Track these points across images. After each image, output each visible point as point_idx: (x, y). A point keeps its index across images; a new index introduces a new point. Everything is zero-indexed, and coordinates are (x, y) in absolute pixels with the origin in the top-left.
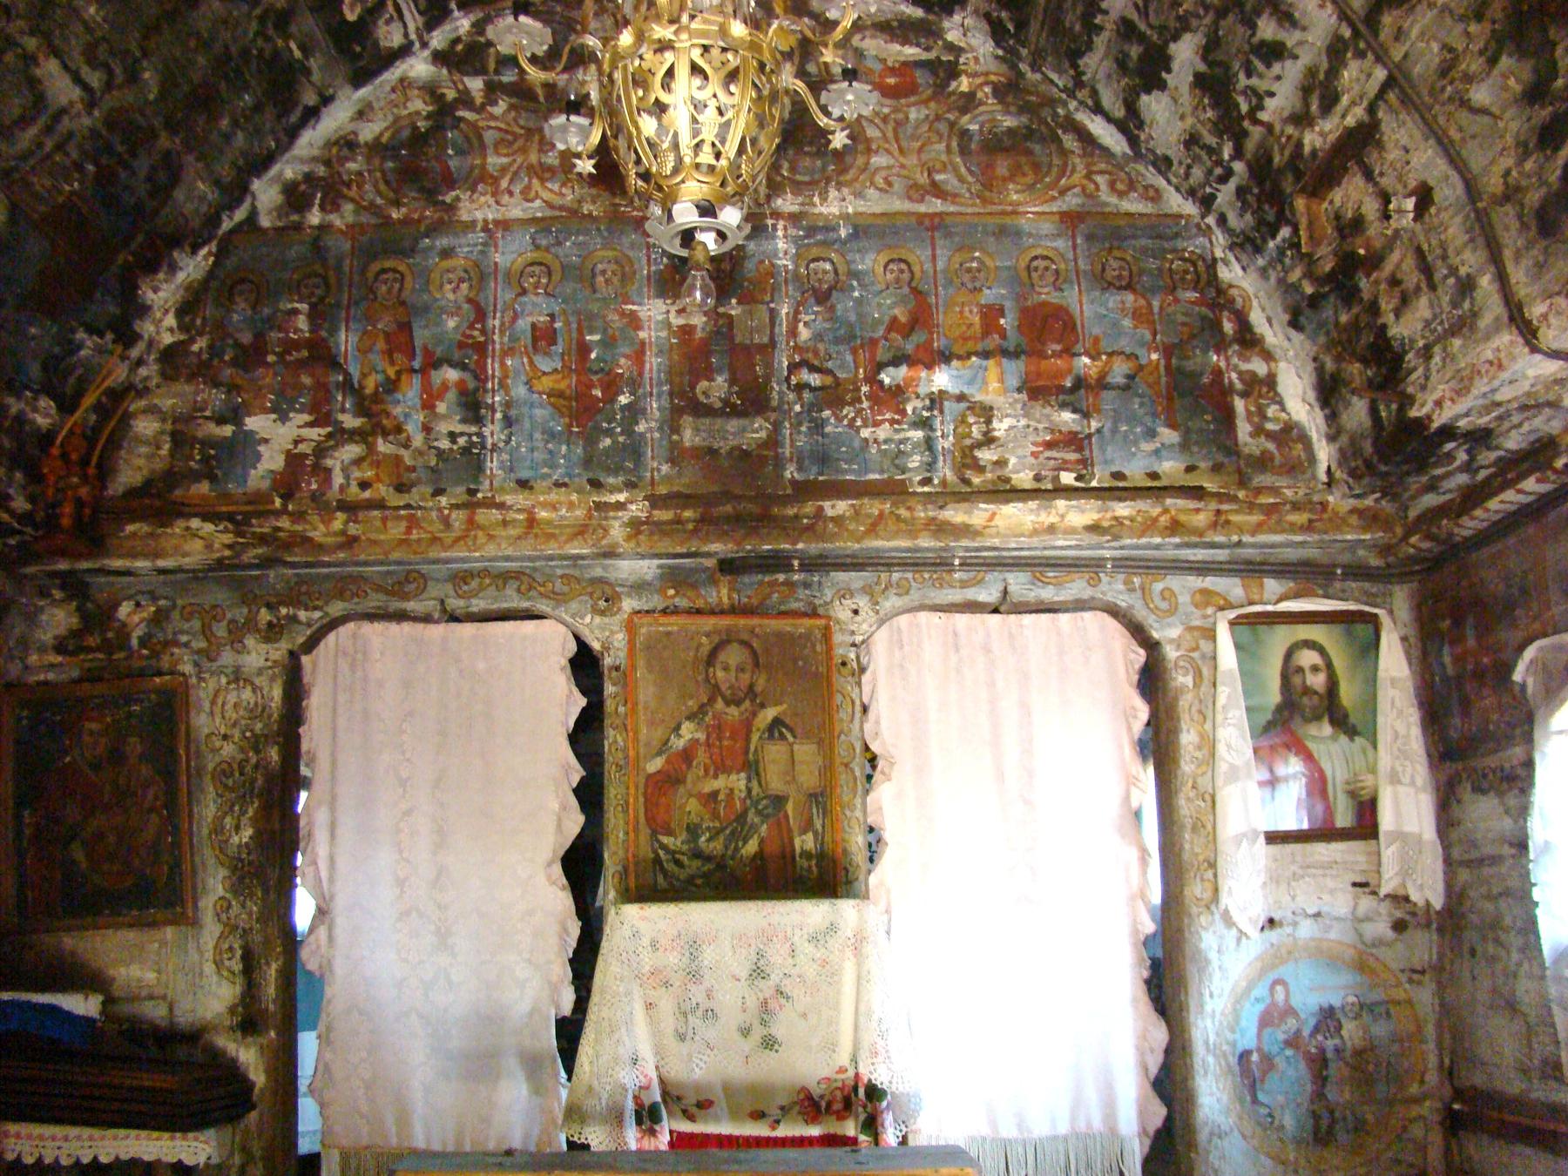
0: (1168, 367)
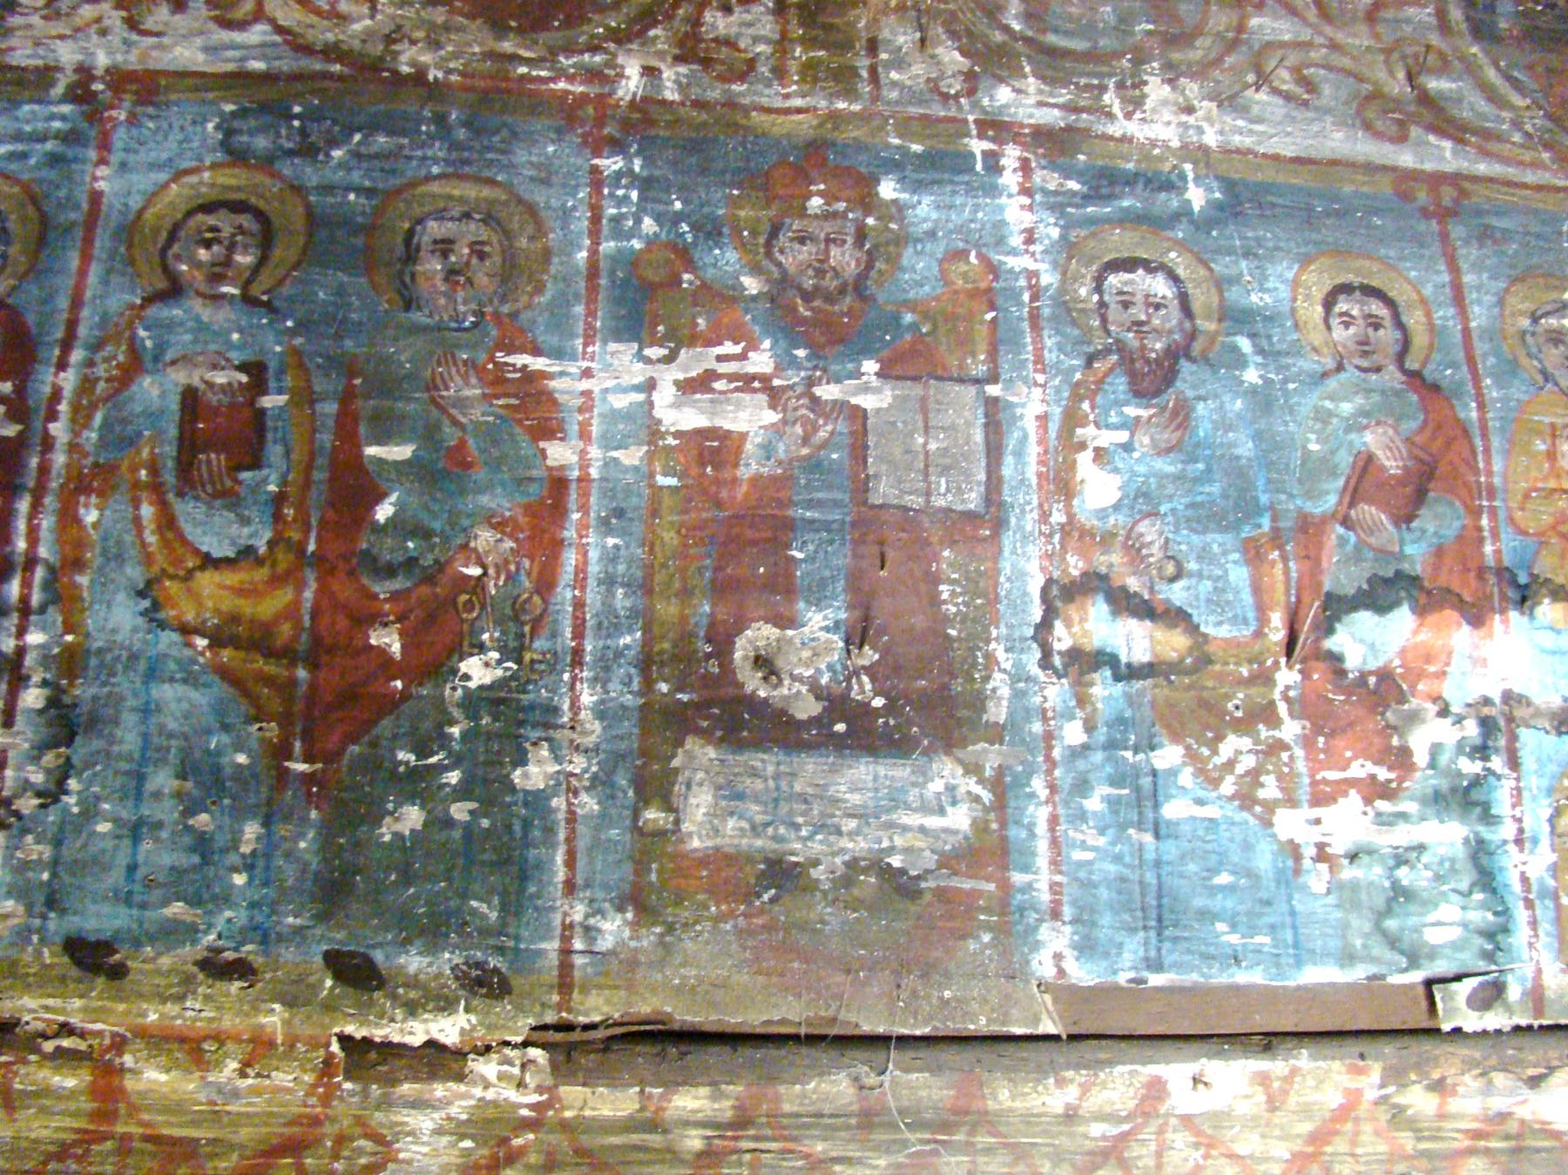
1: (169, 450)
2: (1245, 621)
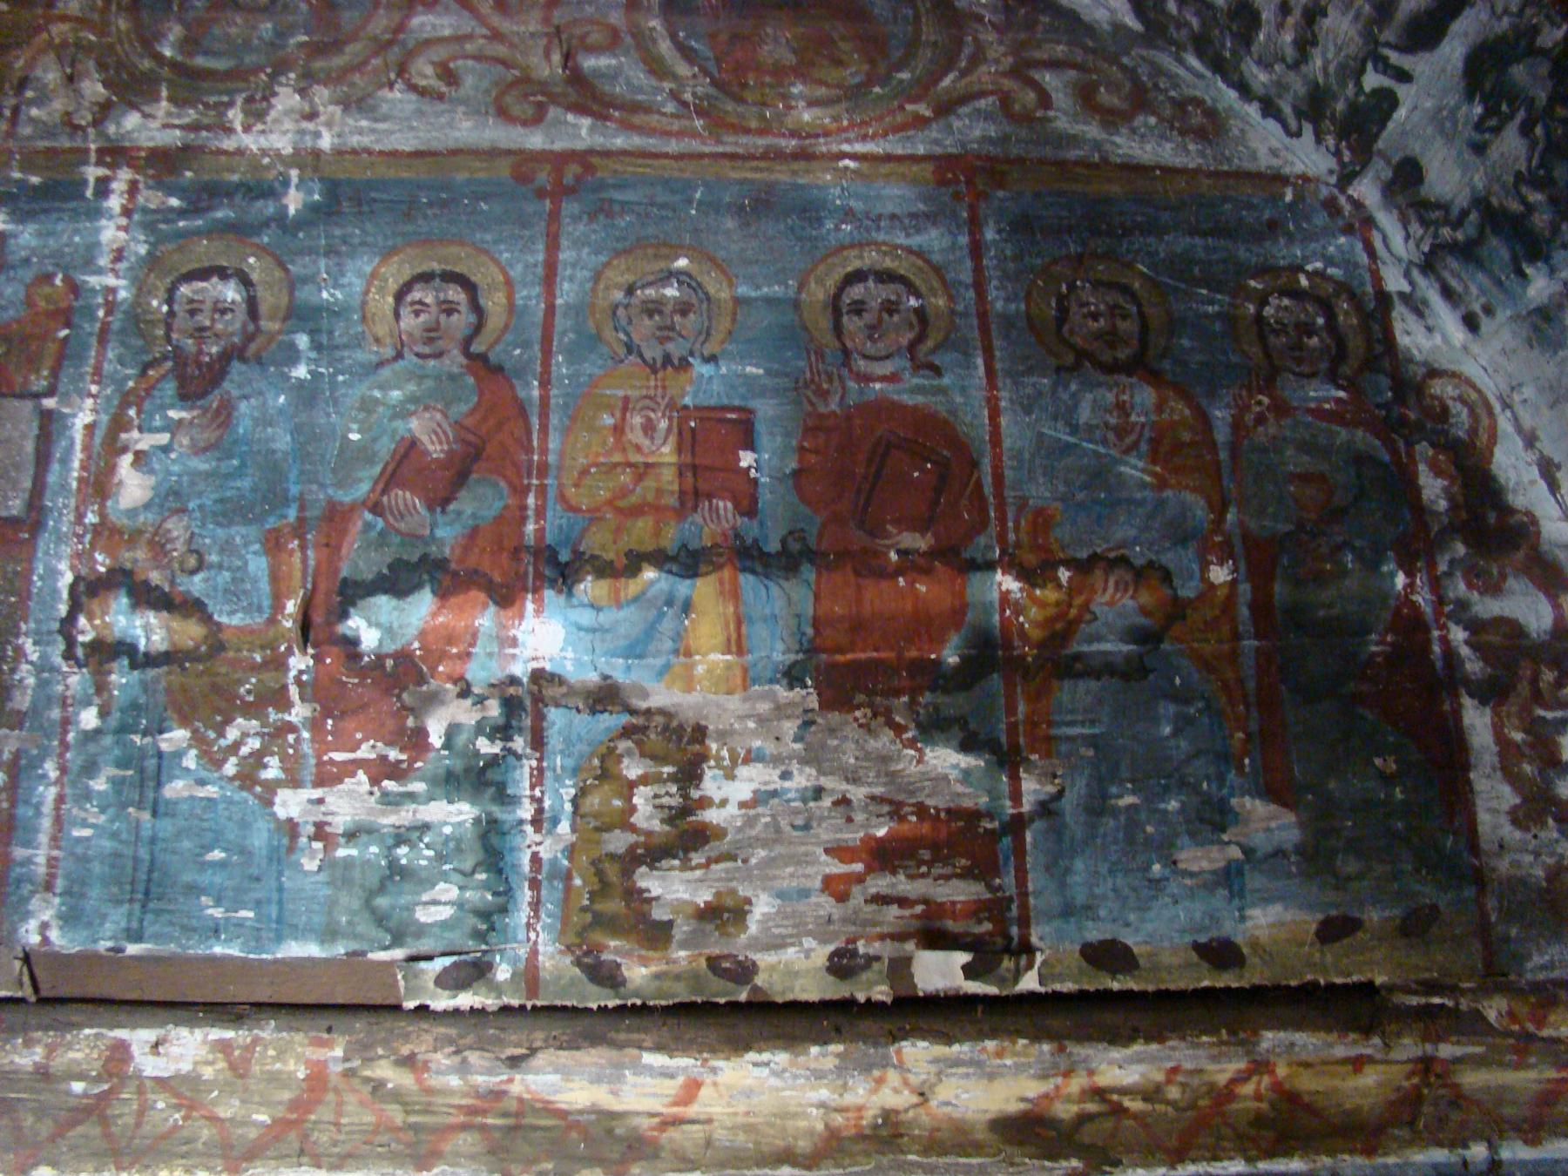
0: (1262, 608)
2: (260, 609)
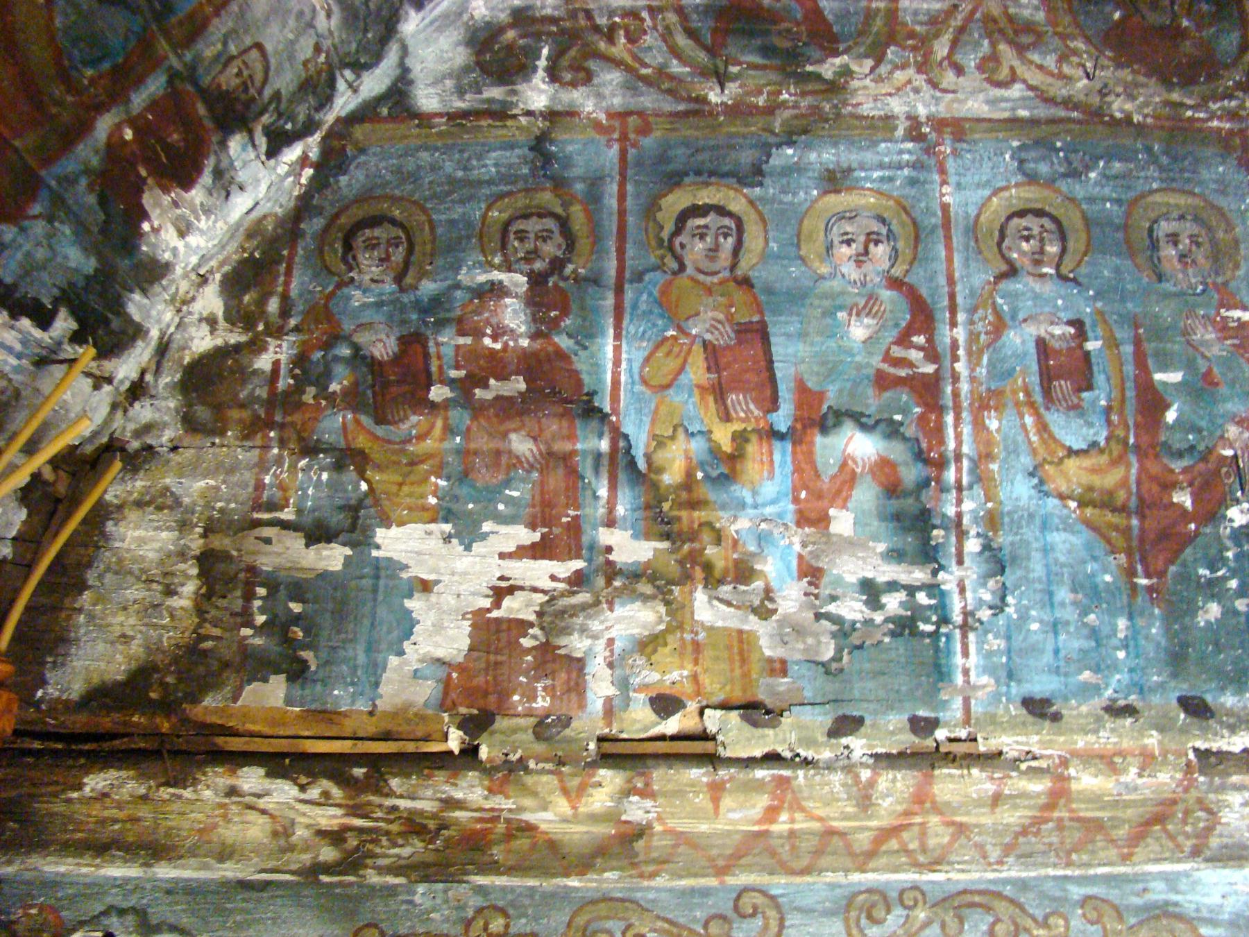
1: (1034, 380)
